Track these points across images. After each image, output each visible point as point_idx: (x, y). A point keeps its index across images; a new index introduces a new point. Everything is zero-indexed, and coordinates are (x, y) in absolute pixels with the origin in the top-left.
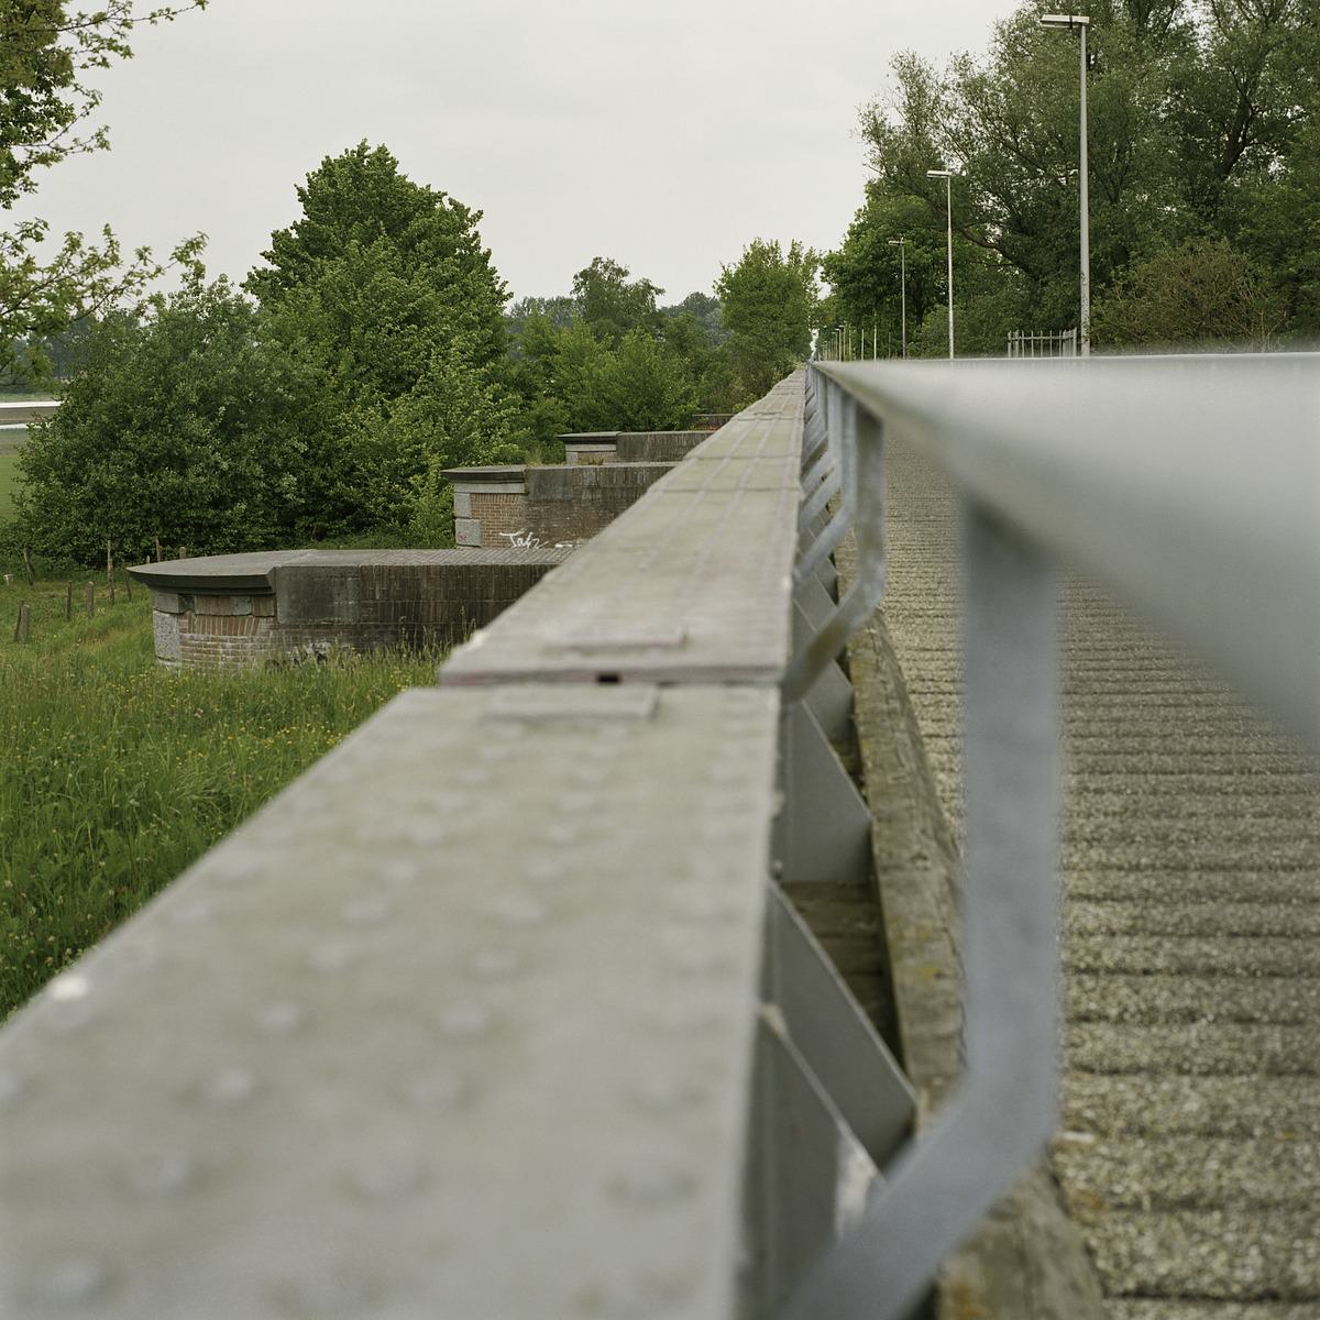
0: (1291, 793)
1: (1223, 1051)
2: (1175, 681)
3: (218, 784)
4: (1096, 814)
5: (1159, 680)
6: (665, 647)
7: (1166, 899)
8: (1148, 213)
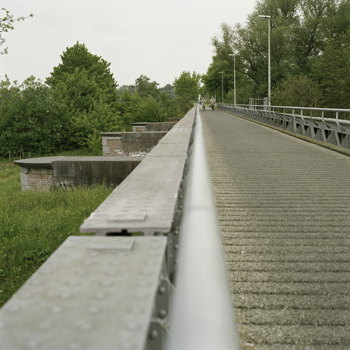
0: (314, 238)
1: (289, 318)
2: (286, 203)
3: (35, 225)
4: (262, 245)
5: (282, 203)
6: (139, 221)
7: (278, 271)
8: (287, 65)
